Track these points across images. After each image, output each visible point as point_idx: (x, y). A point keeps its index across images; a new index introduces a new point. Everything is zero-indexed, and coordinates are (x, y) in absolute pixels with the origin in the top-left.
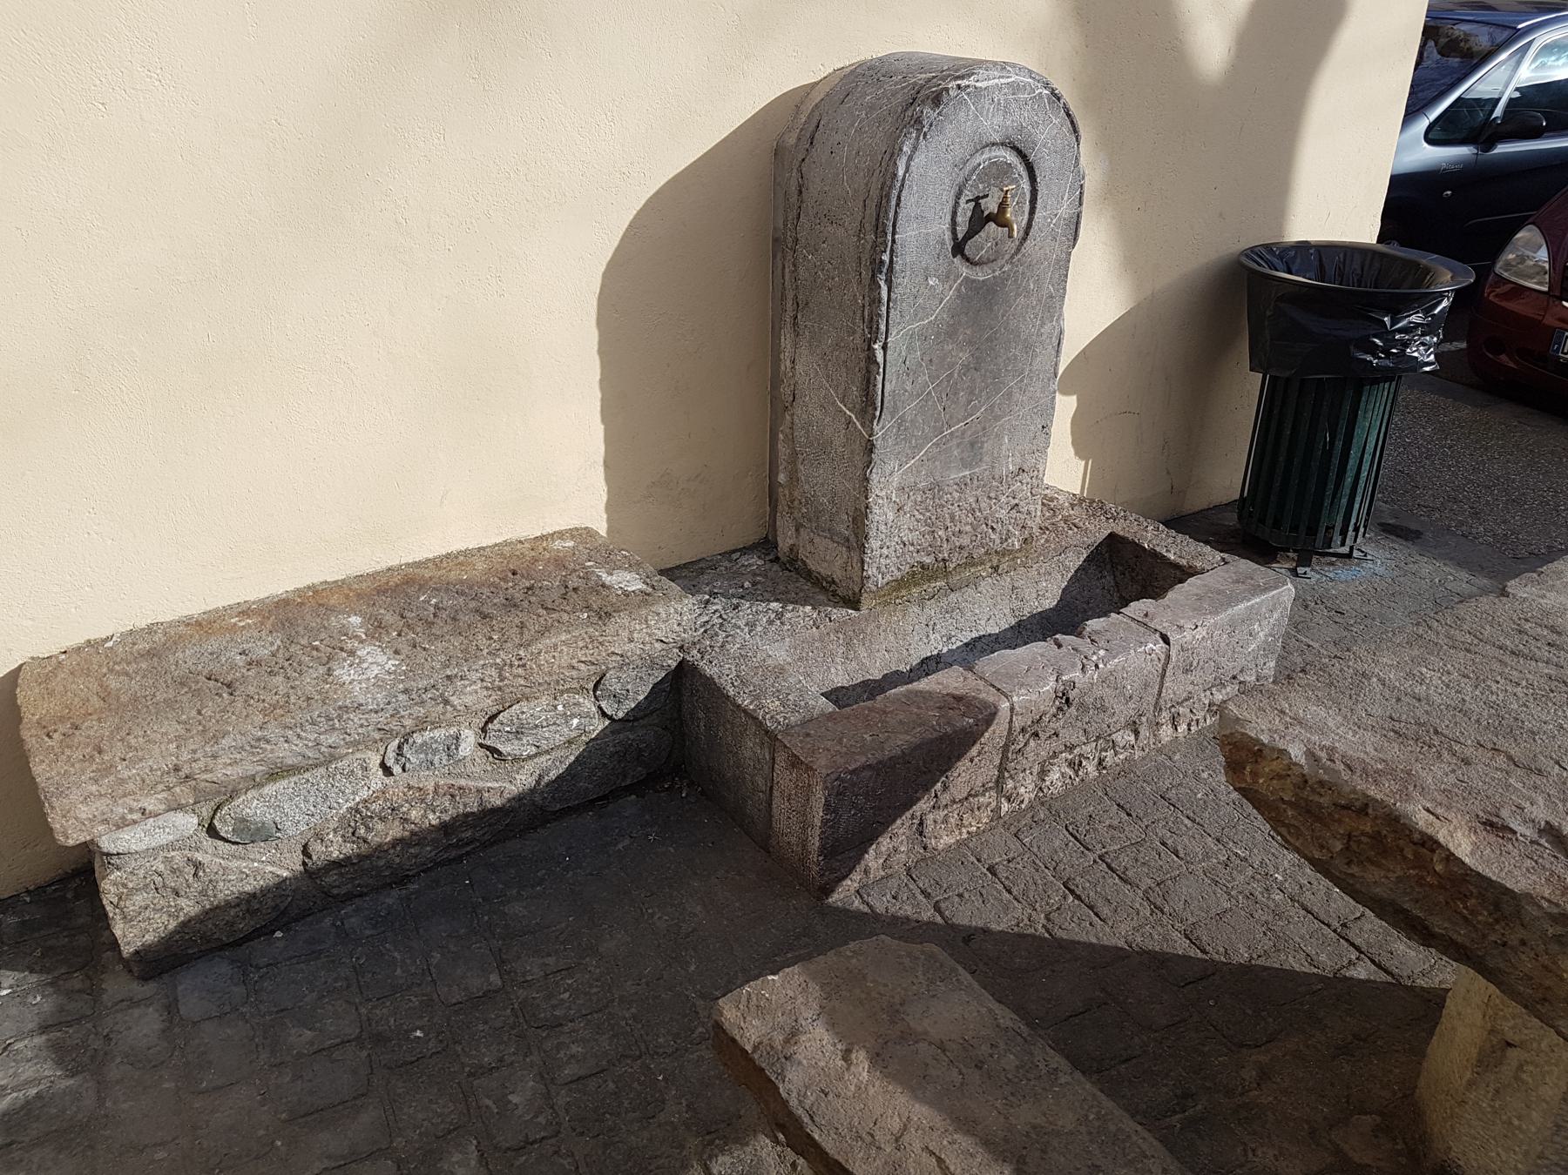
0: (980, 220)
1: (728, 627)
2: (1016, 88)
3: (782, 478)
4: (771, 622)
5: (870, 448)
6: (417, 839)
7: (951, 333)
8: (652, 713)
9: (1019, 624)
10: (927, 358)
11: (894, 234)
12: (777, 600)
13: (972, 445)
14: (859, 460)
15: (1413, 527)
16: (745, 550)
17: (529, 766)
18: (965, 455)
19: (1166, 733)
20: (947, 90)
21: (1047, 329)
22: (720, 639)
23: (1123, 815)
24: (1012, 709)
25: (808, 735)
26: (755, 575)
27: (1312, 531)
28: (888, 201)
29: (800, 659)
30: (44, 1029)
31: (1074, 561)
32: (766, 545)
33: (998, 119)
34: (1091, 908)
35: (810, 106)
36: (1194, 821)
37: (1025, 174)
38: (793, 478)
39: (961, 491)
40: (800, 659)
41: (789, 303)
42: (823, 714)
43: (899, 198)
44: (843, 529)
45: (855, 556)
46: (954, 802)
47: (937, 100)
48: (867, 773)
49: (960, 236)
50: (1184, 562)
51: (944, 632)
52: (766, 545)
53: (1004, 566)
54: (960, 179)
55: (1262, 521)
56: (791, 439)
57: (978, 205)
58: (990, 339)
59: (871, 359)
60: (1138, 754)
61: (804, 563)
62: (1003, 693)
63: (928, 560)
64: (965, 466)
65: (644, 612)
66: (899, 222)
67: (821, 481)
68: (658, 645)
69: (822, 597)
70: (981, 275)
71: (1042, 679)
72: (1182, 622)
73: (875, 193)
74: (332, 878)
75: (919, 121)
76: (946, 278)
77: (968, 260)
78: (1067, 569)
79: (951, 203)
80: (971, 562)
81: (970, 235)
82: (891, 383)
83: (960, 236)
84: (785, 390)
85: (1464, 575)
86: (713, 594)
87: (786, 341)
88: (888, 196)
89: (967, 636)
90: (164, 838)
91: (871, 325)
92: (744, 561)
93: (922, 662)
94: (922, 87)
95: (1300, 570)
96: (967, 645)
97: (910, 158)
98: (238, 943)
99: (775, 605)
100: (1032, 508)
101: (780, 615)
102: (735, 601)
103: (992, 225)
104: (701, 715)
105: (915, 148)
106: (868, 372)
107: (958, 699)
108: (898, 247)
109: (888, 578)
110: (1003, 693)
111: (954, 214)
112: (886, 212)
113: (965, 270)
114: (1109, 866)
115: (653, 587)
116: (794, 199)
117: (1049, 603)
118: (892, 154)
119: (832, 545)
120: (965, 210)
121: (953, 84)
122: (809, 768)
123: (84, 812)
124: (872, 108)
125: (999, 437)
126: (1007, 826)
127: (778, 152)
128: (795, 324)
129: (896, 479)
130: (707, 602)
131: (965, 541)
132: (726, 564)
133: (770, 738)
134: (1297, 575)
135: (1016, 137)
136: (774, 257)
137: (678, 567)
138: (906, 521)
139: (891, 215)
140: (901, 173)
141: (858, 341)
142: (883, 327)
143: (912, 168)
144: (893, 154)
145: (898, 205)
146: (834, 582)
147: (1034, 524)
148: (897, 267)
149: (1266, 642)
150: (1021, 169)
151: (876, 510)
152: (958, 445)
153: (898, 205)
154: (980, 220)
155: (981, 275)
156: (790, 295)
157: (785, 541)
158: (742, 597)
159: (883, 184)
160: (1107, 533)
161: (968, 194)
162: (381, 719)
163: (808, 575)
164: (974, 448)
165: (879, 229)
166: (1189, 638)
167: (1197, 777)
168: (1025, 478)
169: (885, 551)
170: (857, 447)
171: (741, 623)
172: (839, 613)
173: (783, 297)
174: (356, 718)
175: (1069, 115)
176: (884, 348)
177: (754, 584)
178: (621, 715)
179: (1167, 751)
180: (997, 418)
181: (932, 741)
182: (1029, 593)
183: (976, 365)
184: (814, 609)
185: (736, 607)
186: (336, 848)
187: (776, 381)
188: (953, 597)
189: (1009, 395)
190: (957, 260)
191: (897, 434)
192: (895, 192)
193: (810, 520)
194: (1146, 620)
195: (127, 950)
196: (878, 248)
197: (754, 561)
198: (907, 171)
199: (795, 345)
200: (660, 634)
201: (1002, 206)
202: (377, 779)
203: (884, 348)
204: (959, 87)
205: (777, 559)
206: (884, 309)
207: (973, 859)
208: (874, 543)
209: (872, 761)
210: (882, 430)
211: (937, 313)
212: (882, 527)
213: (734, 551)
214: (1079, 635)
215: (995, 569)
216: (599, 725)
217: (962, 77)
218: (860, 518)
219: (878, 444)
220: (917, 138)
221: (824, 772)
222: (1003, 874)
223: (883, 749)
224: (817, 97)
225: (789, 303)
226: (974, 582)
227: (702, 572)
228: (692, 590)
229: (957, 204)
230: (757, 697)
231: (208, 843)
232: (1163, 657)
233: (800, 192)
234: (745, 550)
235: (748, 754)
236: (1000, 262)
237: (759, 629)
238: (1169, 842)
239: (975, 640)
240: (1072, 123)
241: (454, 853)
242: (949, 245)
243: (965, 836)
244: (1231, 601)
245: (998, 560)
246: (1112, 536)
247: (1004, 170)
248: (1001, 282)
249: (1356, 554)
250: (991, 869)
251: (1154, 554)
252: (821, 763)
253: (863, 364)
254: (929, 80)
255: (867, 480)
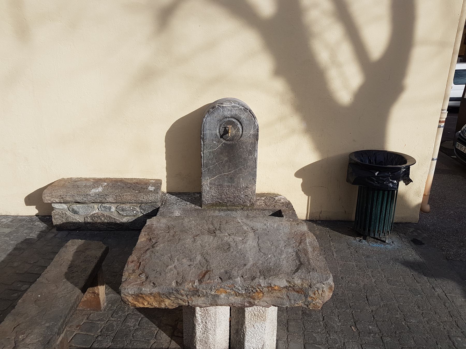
2: (233, 107)
6: (103, 223)
17: (126, 218)
30: (41, 232)
74: (88, 225)
90: (61, 208)
98: (71, 230)
123: (47, 198)
125: (239, 178)
162: (94, 198)
164: (231, 179)
174: (89, 197)
186: (89, 220)
189: (241, 169)
195: (54, 224)
202: (97, 211)
226: (236, 210)
231: (68, 211)
241: (110, 229)
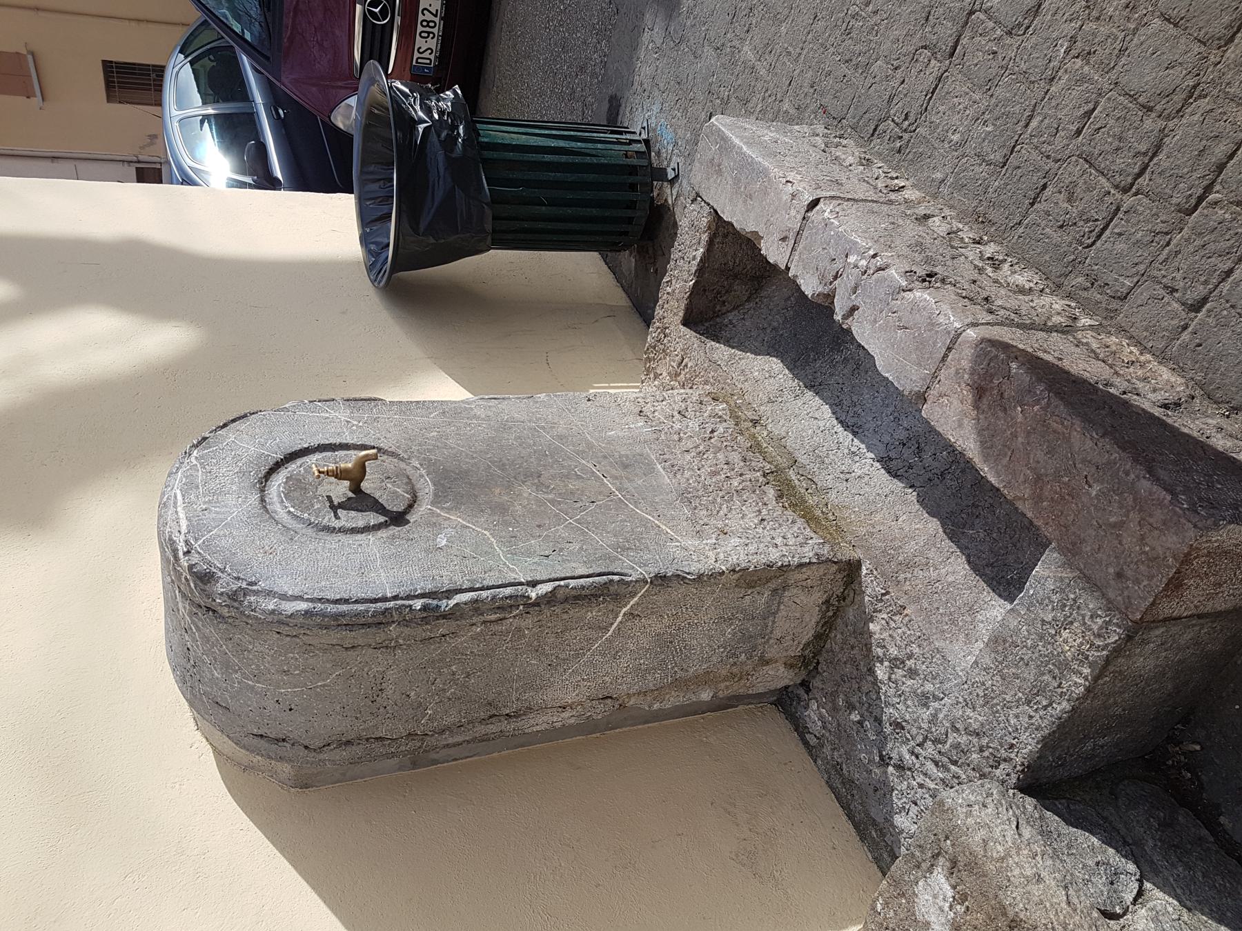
0: (360, 500)
1: (938, 731)
2: (190, 486)
3: (706, 696)
4: (912, 673)
5: (661, 580)
7: (502, 509)
8: (1105, 819)
9: (810, 387)
10: (537, 532)
11: (384, 599)
12: (871, 671)
13: (625, 467)
14: (677, 592)
15: (606, 106)
16: (800, 729)
18: (638, 471)
19: (909, 194)
20: (191, 567)
21: (480, 412)
22: (963, 739)
23: (1048, 192)
24: (974, 325)
25: (1119, 575)
26: (835, 709)
27: (633, 170)
28: (343, 615)
29: (953, 622)
31: (721, 352)
32: (786, 702)
33: (230, 500)
34: (1221, 167)
35: (241, 754)
36: (1031, 117)
37: (299, 461)
38: (705, 679)
39: (682, 469)
40: (953, 622)
41: (493, 728)
42: (1068, 564)
43: (337, 602)
44: (762, 599)
45: (795, 577)
46: (1116, 373)
47: (205, 578)
48: (1162, 474)
49: (382, 519)
50: (705, 237)
51: (848, 461)
52: (786, 702)
53: (750, 414)
54: (310, 531)
55: (630, 220)
56: (659, 691)
57: (341, 506)
58: (502, 467)
59: (549, 599)
60: (947, 212)
61: (807, 645)
62: (954, 341)
63: (771, 492)
64: (650, 470)
65: (991, 867)
66: (370, 595)
67: (706, 639)
68: (1027, 832)
69: (851, 613)
70: (427, 488)
71: (915, 307)
72: (786, 198)
73: (334, 636)
75: (233, 596)
76: (434, 525)
77: (411, 506)
78: (732, 357)
79: (341, 537)
80: (756, 447)
81: (378, 507)
82: (575, 566)
83: (382, 519)
84: (600, 711)
85: (646, 37)
86: (884, 761)
87: (538, 723)
88: (336, 616)
89: (846, 437)
91: (511, 605)
92: (816, 726)
93: (896, 476)
94: (192, 602)
95: (671, 175)
96: (855, 434)
97: (284, 597)
99: (881, 672)
100: (678, 398)
101: (896, 663)
102: (888, 729)
103: (366, 486)
104: (1089, 745)
105: (269, 593)
106: (566, 600)
107: (980, 392)
108: (403, 591)
109: (808, 532)
110: (954, 341)
111: (354, 531)
112: (358, 615)
113: (423, 508)
114: (1140, 174)
115: (936, 856)
116: (357, 750)
117: (775, 364)
118: (280, 622)
119: (783, 613)
120: (349, 518)
121: (184, 562)
122: (1186, 560)
124: (227, 666)
125: (610, 442)
126: (1111, 314)
127: (303, 783)
128: (517, 715)
129: (691, 543)
130: (900, 767)
131: (735, 457)
132: (827, 750)
133: (1135, 633)
134: (677, 177)
135: (253, 477)
136: (435, 762)
137: (850, 816)
138: (734, 523)
139: (361, 607)
140: (303, 606)
141: (529, 621)
142: (508, 591)
143: (297, 592)
144: (279, 622)
145: (346, 601)
146: (827, 602)
147: (695, 395)
148: (429, 587)
149: (777, 131)
150: (293, 467)
151: (733, 559)
152: (630, 480)
153: (346, 601)
154: (360, 500)
155: (427, 488)
156: (481, 730)
157: (779, 676)
158: (878, 721)
159: (321, 627)
160: (683, 329)
161: (328, 519)
163: (820, 638)
165: (381, 621)
166: (803, 184)
167: (962, 143)
168: (648, 409)
169: (779, 541)
170: (660, 599)
171: (926, 714)
172: (871, 585)
173: (485, 739)
175: (225, 425)
176: (533, 584)
177: (851, 707)
178: (1131, 867)
179: (934, 190)
180: (590, 446)
181: (1068, 404)
182: (771, 386)
183: (534, 477)
184: (871, 620)
185: (898, 726)
187: (588, 727)
188: (803, 459)
189: (561, 438)
190: (412, 518)
191: (637, 549)
192: (331, 608)
193: (754, 648)
194: (792, 236)
196: (405, 618)
197: (814, 714)
198: (300, 598)
199: (543, 709)
200: (1011, 833)
201: (340, 475)
203: (533, 584)
204: (187, 553)
205: (805, 685)
206: (484, 594)
207: (1185, 336)
208: (774, 555)
209: (1140, 470)
210: (636, 568)
211: (481, 529)
212: (752, 548)
213: (806, 743)
214: (830, 297)
215: (755, 423)
216: (1159, 898)
217: (175, 551)
218: (747, 579)
219: (653, 570)
220: (256, 593)
221: (1191, 533)
222: (1201, 291)
223: (1111, 464)
224: (229, 746)
225: (493, 728)
226: (779, 442)
227: (849, 782)
228: (883, 790)
229: (342, 530)
230: (1064, 666)
232: (835, 202)
233: (348, 743)
234: (800, 729)
235: (1151, 663)
236: (410, 471)
237: (929, 687)
238: (1074, 128)
239: (846, 426)
240: (234, 421)
242: (394, 530)
243: (1149, 357)
244: (746, 164)
245: (746, 422)
246: (685, 323)
247: (296, 488)
248: (429, 464)
249: (644, 136)
250: (1196, 307)
251: (700, 271)
252: (1171, 542)
253: (558, 610)
254: (184, 596)
255: (700, 576)
